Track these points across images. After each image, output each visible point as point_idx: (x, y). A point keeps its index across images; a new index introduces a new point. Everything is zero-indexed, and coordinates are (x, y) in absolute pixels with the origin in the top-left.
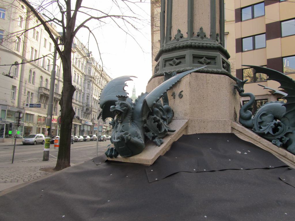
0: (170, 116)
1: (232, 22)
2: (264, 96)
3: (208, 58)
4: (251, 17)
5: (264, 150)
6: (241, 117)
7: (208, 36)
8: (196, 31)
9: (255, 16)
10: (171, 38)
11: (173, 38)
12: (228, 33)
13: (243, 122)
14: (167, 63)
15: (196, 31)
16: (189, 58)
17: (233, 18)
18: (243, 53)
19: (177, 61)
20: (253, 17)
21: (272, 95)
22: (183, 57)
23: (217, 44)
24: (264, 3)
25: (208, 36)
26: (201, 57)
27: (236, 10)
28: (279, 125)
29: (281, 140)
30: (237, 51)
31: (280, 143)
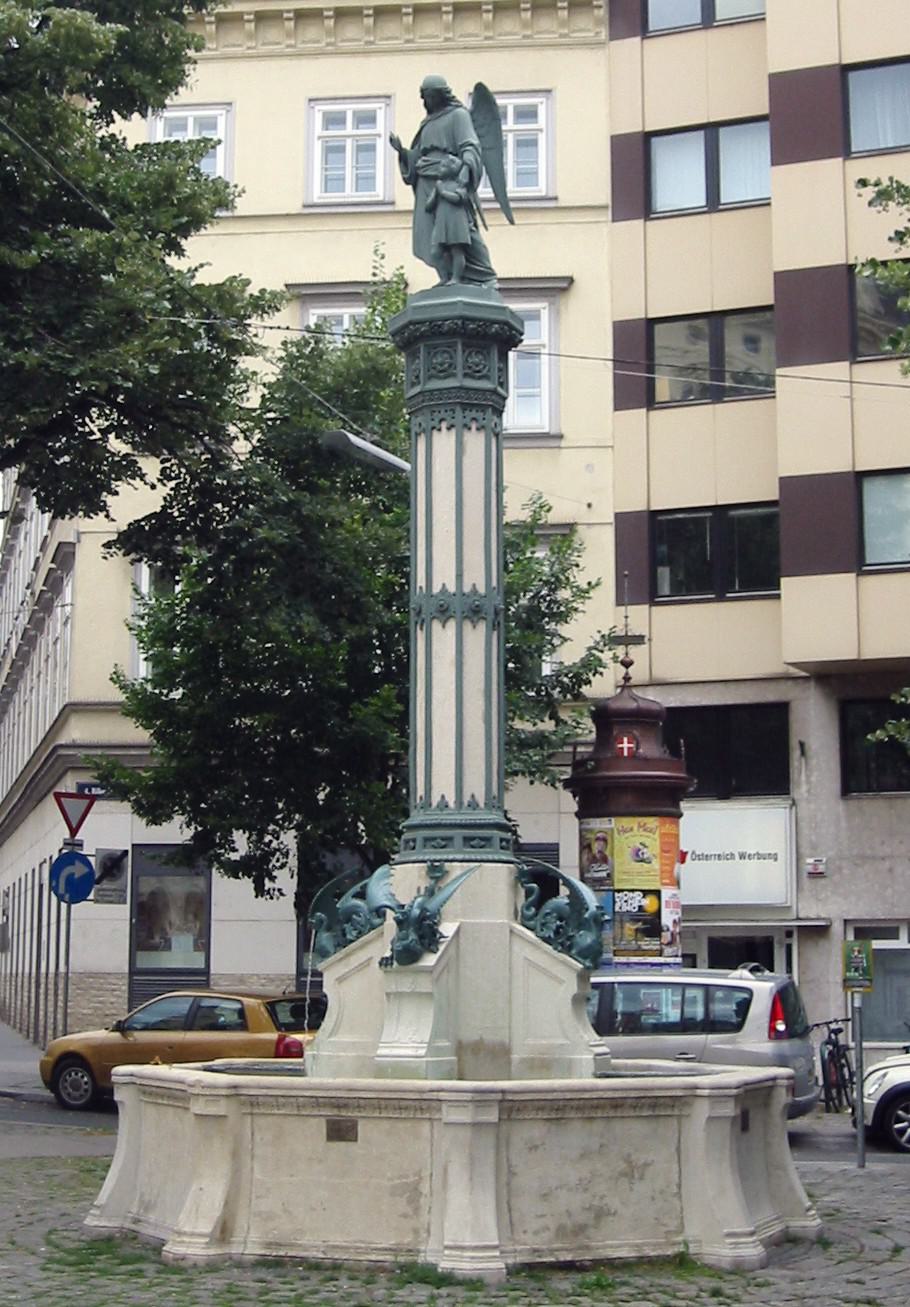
0: (377, 921)
1: (590, 217)
2: (772, 686)
3: (482, 839)
4: (700, 200)
5: (743, 1065)
6: (523, 915)
7: (482, 805)
8: (467, 799)
9: (727, 196)
10: (430, 805)
11: (434, 804)
12: (565, 285)
13: (527, 923)
14: (429, 844)
15: (467, 799)
16: (458, 841)
17: (601, 191)
18: (653, 413)
19: (443, 843)
20: (713, 203)
21: (812, 684)
22: (450, 839)
23: (496, 817)
24: (771, 124)
25: (482, 805)
26: (473, 839)
27: (619, 144)
28: (561, 927)
29: (562, 944)
30: (622, 402)
31: (560, 948)
